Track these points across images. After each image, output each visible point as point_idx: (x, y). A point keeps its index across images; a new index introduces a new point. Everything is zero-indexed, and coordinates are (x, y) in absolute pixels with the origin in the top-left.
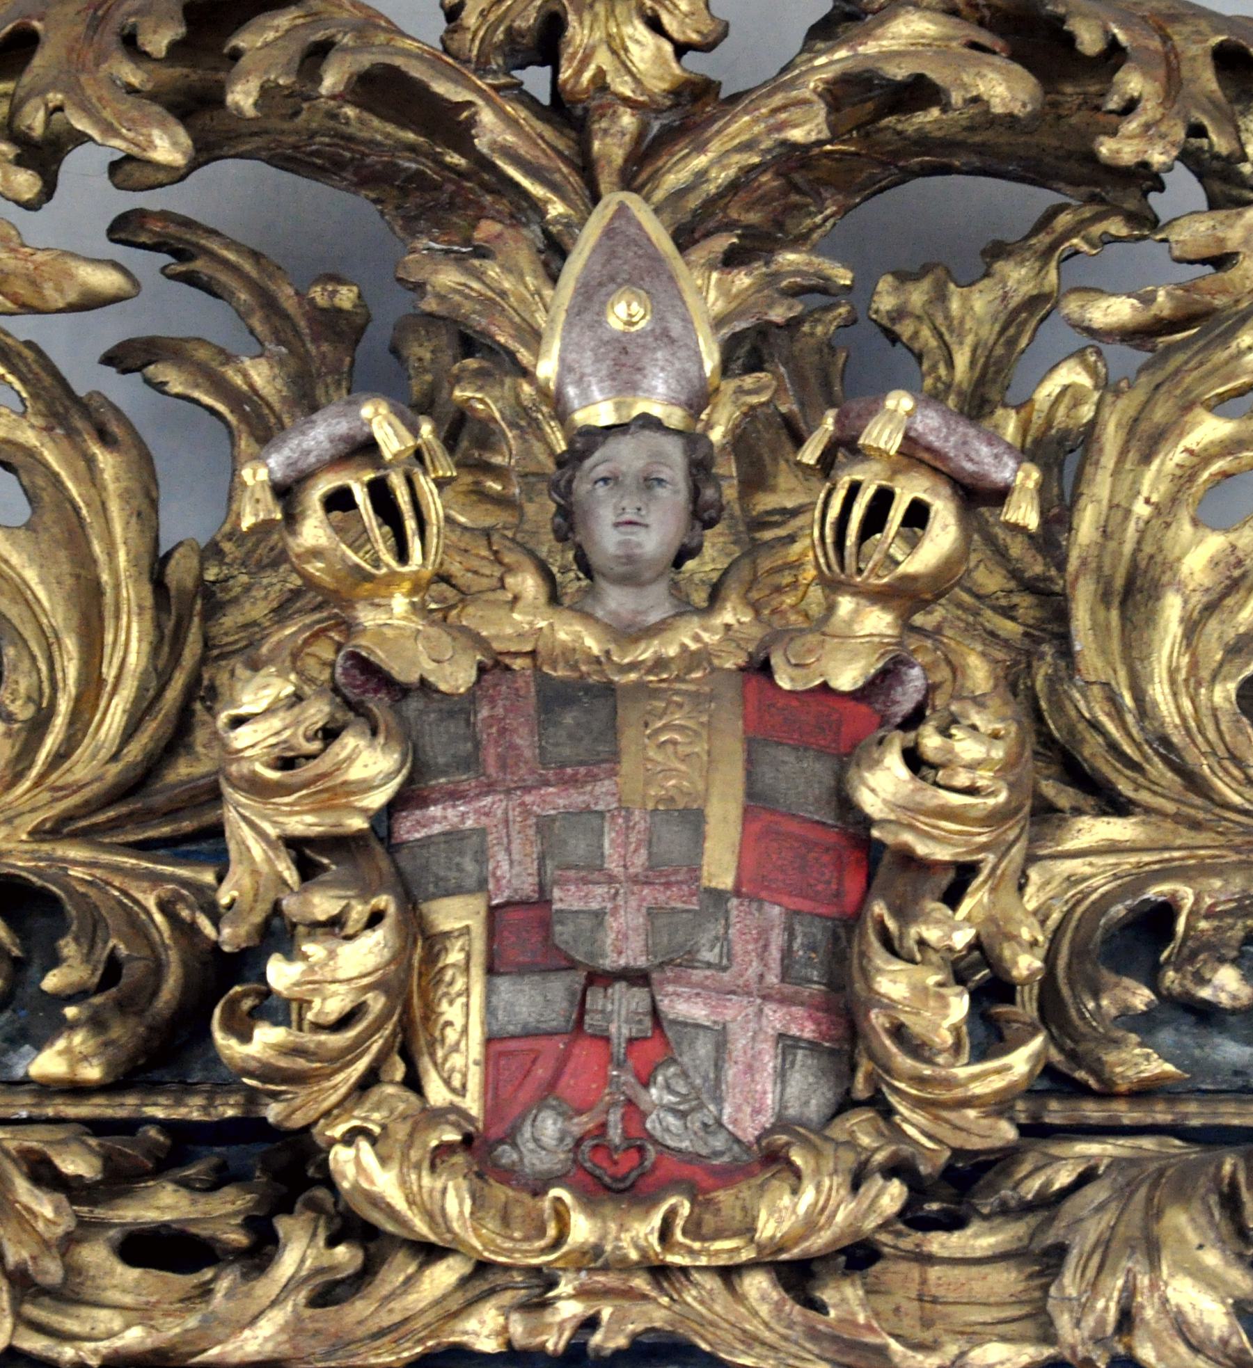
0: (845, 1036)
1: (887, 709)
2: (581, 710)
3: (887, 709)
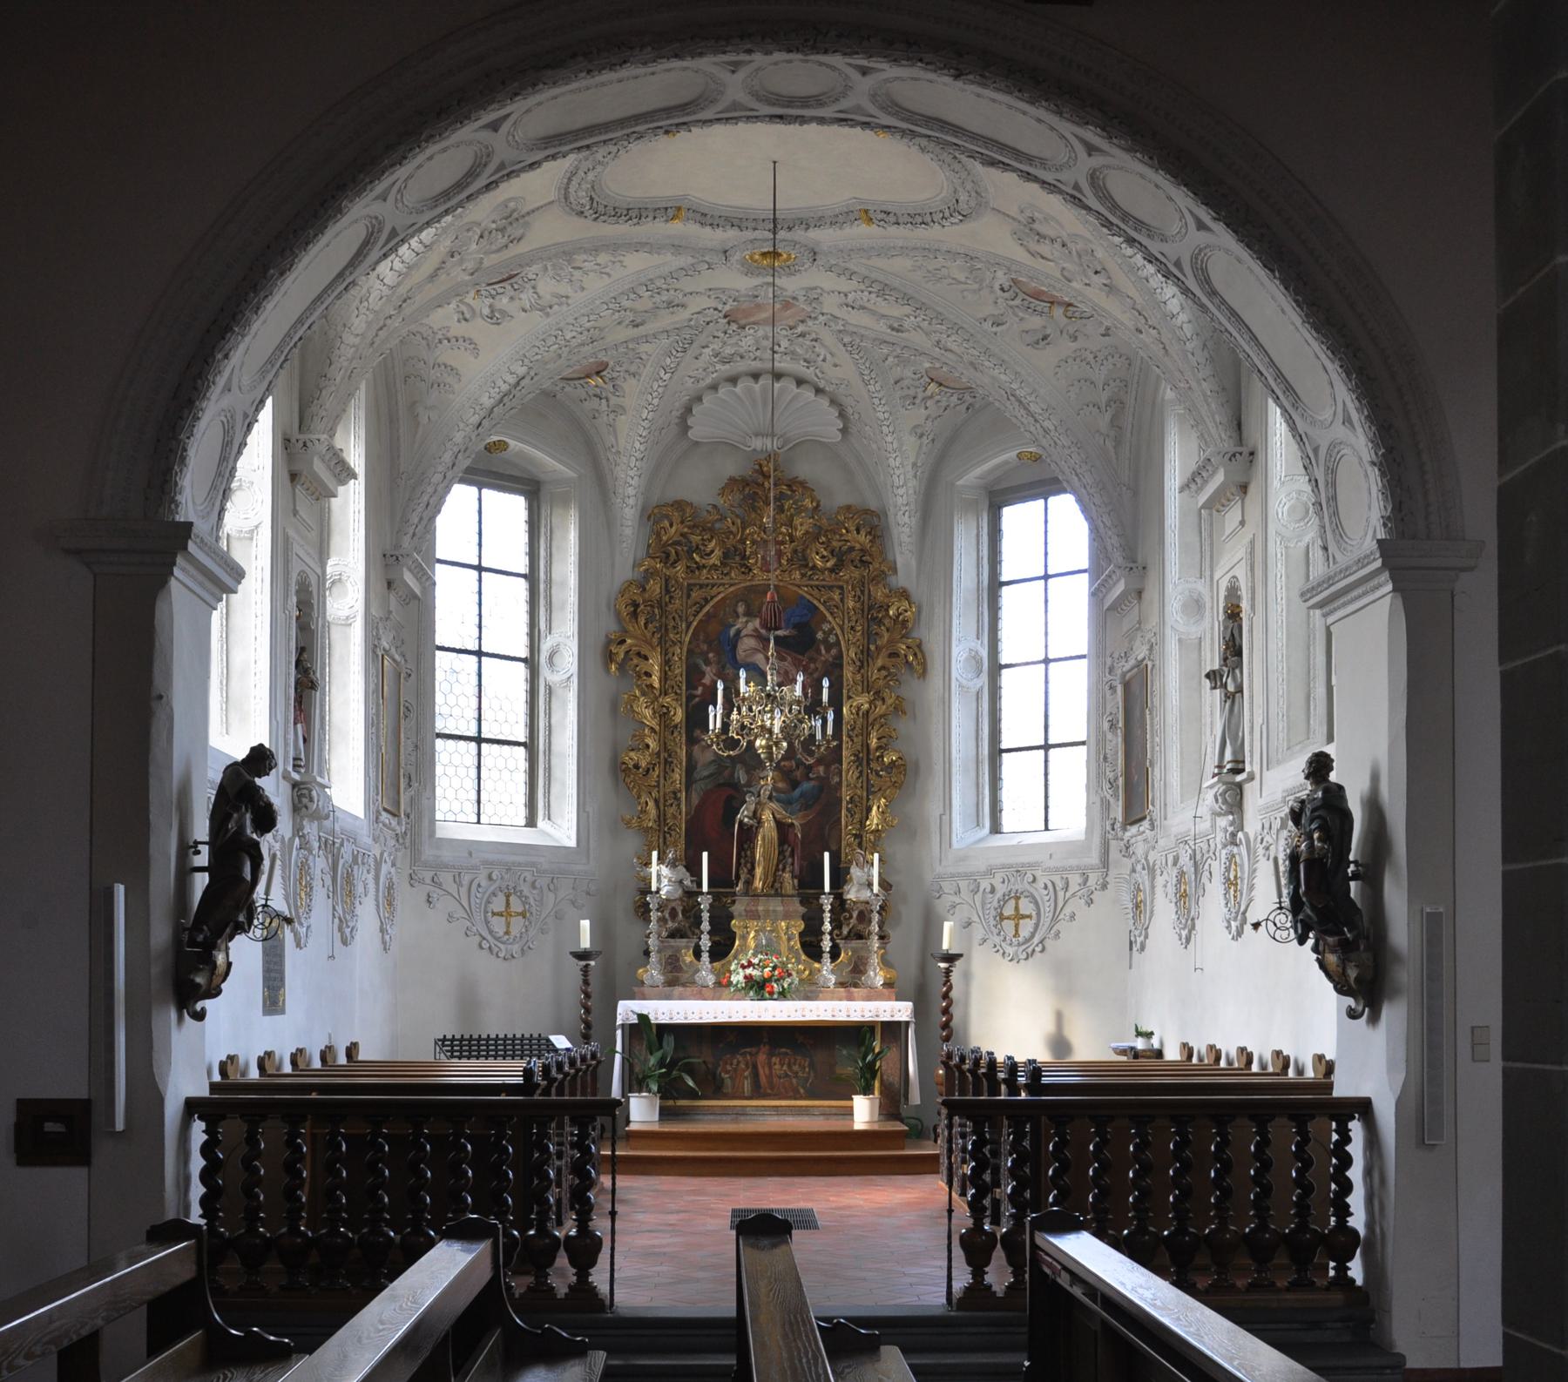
0: (780, 564)
1: (782, 543)
2: (766, 542)
3: (782, 543)
